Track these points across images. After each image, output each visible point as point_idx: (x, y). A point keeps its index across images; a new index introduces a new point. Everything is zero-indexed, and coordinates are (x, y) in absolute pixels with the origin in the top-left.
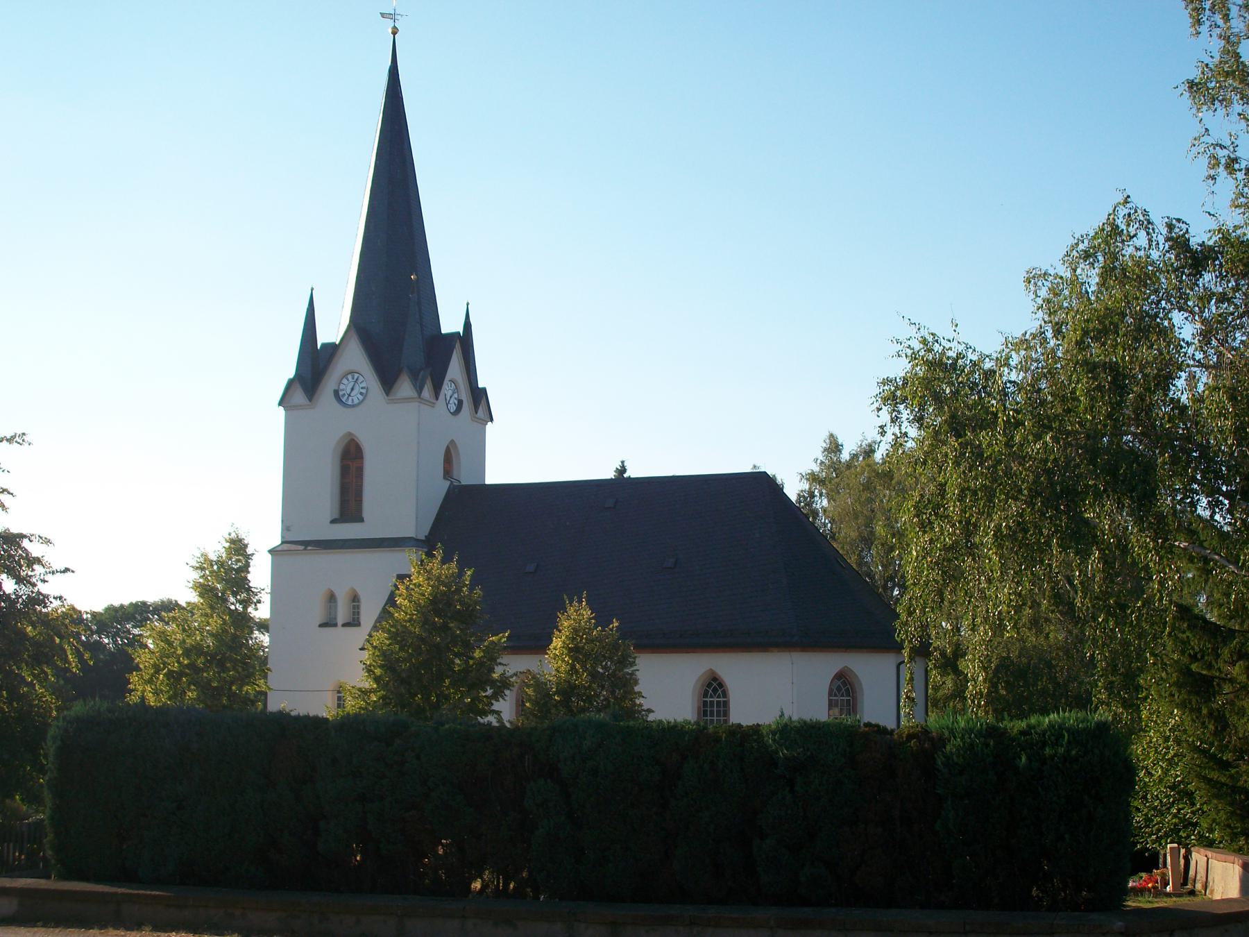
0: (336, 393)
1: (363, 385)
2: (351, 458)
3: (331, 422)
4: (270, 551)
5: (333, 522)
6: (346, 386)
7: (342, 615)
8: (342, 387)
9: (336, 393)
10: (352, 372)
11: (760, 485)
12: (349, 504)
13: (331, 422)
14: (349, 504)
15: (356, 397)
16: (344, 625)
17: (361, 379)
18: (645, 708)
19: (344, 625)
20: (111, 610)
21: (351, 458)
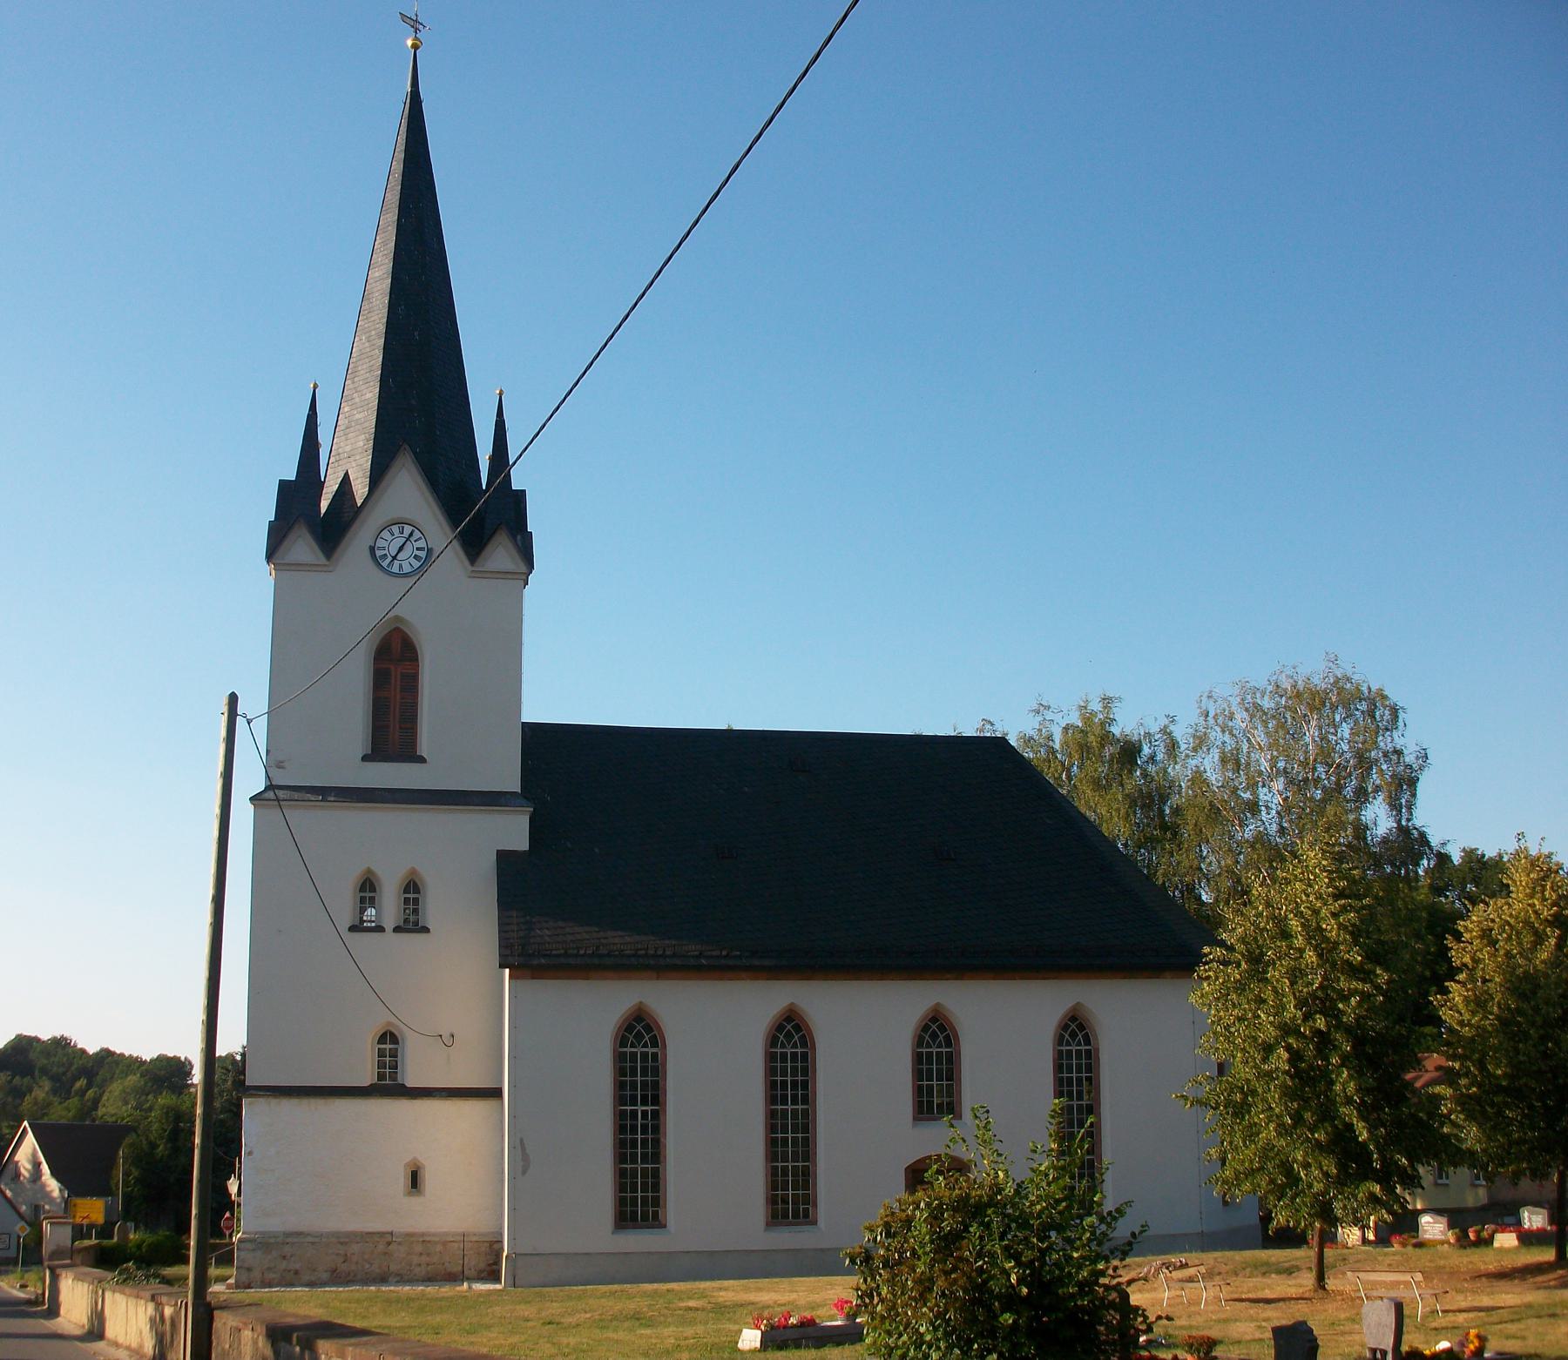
0: (372, 549)
1: (422, 544)
2: (395, 660)
3: (358, 596)
4: (251, 799)
5: (365, 758)
6: (390, 543)
7: (389, 908)
8: (380, 543)
9: (372, 549)
10: (401, 523)
11: (1001, 743)
12: (393, 726)
13: (358, 596)
14: (393, 726)
15: (407, 562)
16: (397, 929)
17: (417, 534)
18: (1396, 1241)
19: (397, 929)
20: (106, 1054)
21: (395, 660)
